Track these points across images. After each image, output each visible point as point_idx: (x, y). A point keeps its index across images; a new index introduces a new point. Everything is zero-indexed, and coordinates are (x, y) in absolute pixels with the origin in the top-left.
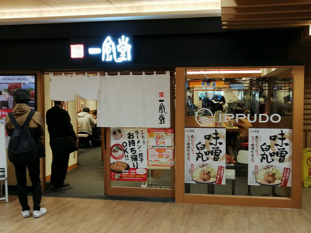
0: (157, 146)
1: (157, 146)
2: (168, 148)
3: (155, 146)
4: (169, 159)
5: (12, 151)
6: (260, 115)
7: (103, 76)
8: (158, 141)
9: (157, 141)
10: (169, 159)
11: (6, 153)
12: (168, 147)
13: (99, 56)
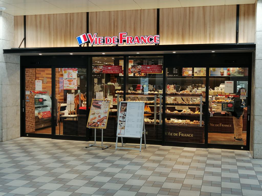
0: (68, 79)
1: (68, 79)
2: (74, 79)
3: (67, 79)
4: (74, 85)
5: (62, 118)
6: (123, 37)
7: (256, 48)
8: (69, 76)
9: (68, 75)
10: (74, 85)
11: (253, 129)
12: (74, 79)
13: (57, 126)
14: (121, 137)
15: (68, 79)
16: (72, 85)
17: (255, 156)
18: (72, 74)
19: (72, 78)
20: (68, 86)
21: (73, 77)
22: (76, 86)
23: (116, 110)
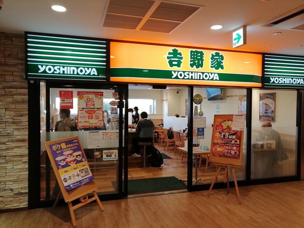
2: (98, 110)
8: (88, 104)
9: (87, 103)
10: (99, 120)
12: (98, 109)
14: (146, 166)
15: (87, 110)
16: (94, 119)
17: (186, 91)
18: (94, 101)
19: (93, 108)
20: (86, 122)
21: (96, 106)
22: (101, 120)
23: (145, 146)
